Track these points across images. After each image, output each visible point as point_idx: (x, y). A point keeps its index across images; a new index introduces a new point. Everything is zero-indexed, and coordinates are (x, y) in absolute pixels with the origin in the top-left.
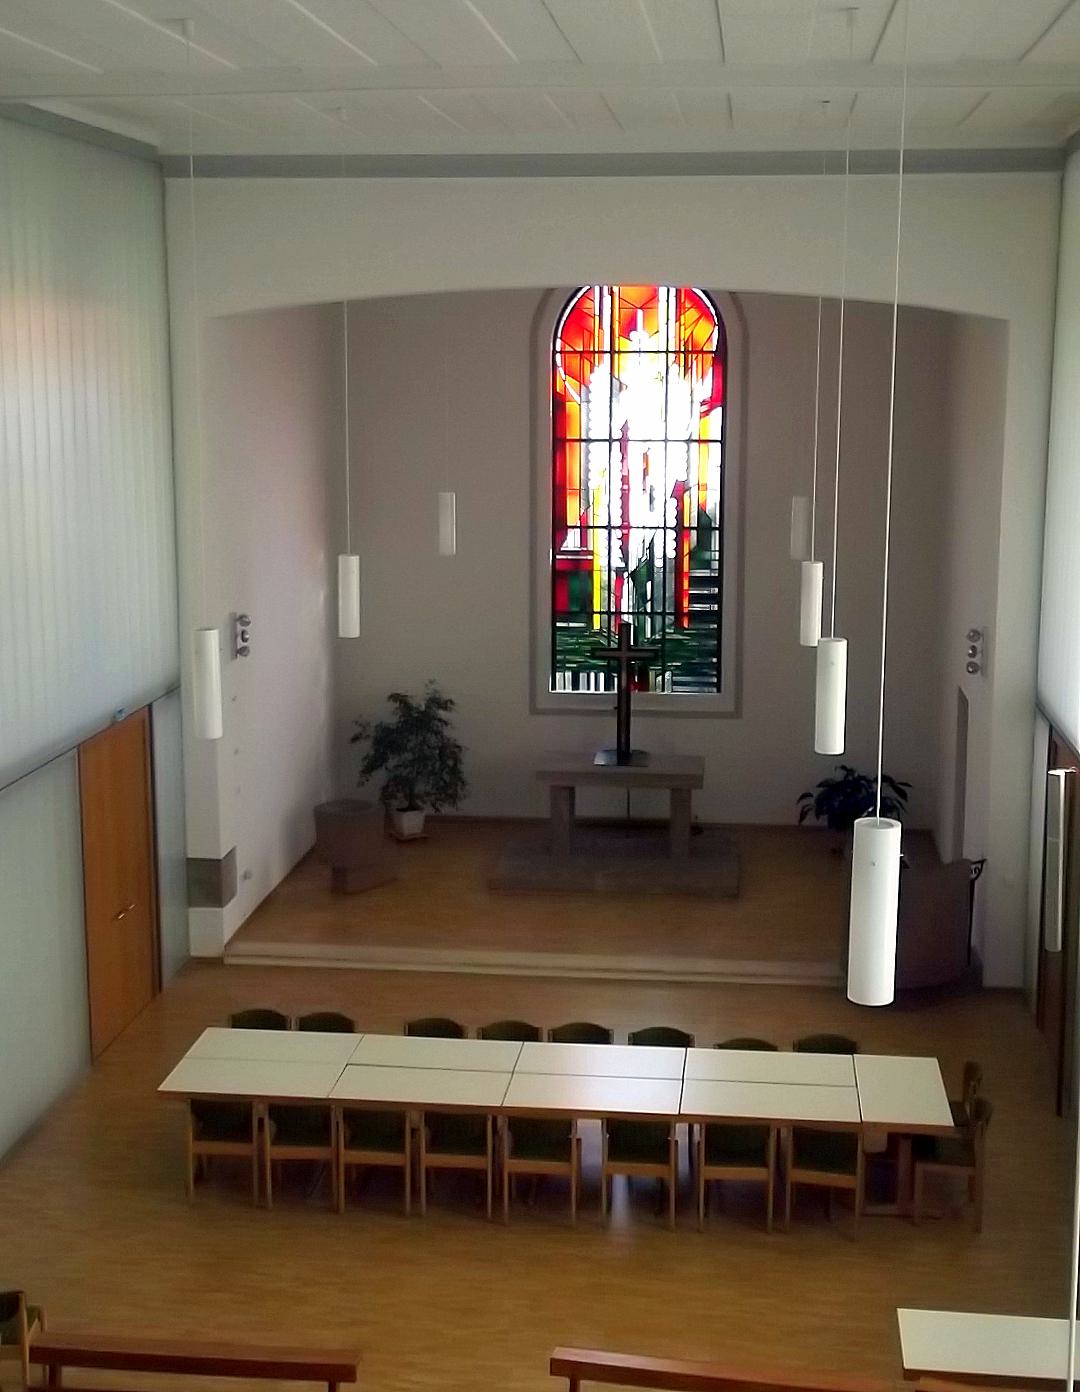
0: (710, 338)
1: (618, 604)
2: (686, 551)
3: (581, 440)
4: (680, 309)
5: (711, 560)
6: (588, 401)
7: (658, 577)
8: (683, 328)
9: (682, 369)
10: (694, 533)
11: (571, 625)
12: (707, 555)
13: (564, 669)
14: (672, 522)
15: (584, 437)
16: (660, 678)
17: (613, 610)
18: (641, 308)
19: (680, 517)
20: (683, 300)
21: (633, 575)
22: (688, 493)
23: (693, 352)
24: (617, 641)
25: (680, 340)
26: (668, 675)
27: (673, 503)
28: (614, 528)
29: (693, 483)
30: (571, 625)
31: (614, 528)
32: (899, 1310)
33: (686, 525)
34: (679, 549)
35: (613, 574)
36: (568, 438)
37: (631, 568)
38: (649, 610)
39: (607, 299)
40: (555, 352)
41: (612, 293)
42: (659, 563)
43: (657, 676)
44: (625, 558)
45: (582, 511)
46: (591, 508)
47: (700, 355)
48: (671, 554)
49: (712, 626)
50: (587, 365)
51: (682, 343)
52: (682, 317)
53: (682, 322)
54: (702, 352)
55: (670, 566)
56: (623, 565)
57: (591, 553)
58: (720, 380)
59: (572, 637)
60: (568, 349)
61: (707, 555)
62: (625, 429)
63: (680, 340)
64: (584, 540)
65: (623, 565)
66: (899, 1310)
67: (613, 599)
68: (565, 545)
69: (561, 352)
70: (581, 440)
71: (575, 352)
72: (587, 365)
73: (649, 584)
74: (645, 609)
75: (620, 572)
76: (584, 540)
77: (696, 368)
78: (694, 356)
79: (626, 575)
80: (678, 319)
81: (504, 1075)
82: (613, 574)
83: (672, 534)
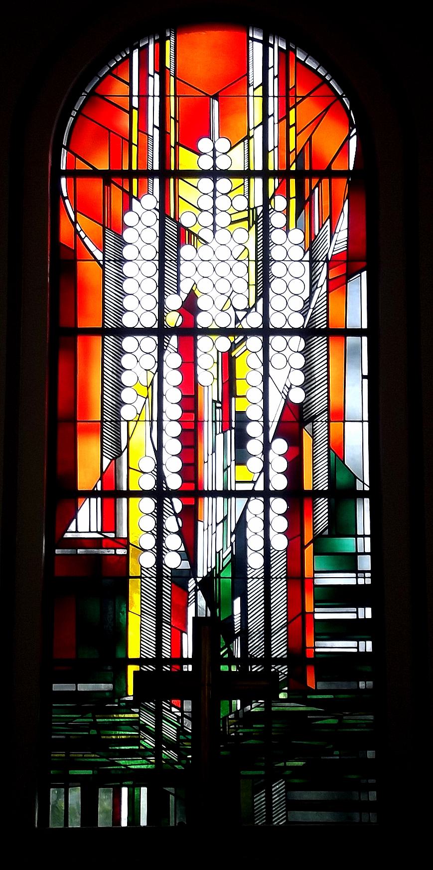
0: (344, 147)
1: (177, 645)
2: (308, 536)
3: (103, 332)
4: (287, 101)
5: (357, 554)
6: (121, 261)
7: (255, 588)
8: (292, 131)
9: (293, 202)
10: (323, 504)
11: (82, 687)
12: (347, 544)
13: (67, 783)
14: (279, 483)
15: (110, 324)
16: (261, 798)
17: (166, 654)
18: (216, 97)
19: (294, 471)
20: (292, 84)
21: (208, 585)
22: (308, 427)
23: (312, 174)
24: (173, 50)
25: (288, 153)
26: (278, 787)
27: (280, 446)
28: (146, 332)
29: (319, 404)
30: (82, 687)
31: (146, 332)
32: (190, 568)
33: (308, 486)
34: (294, 533)
35: (167, 584)
36: (80, 325)
37: (202, 572)
38: (238, 655)
39: (154, 84)
40: (59, 174)
41: (162, 70)
42: (255, 561)
43: (256, 790)
44: (190, 552)
45: (106, 462)
46: (125, 455)
47: (325, 182)
48: (280, 543)
49: (362, 685)
50: (117, 195)
51: (292, 157)
52: (292, 113)
53: (292, 122)
54: (330, 174)
55: (279, 567)
56: (186, 565)
57: (125, 543)
58: (116, 616)
59: (83, 712)
60: (80, 165)
61: (347, 544)
62: (190, 307)
63: (288, 153)
64: (110, 519)
65: (186, 565)
66: (190, 568)
67: (166, 633)
68: (72, 527)
69: (67, 173)
70: (103, 332)
71: (95, 173)
72: (117, 195)
73: (237, 602)
74: (230, 652)
75: (180, 578)
76: (110, 519)
77: (319, 196)
78: (315, 181)
79: (192, 584)
80: (284, 116)
81: (241, 186)
82: (167, 584)
83: (279, 505)
